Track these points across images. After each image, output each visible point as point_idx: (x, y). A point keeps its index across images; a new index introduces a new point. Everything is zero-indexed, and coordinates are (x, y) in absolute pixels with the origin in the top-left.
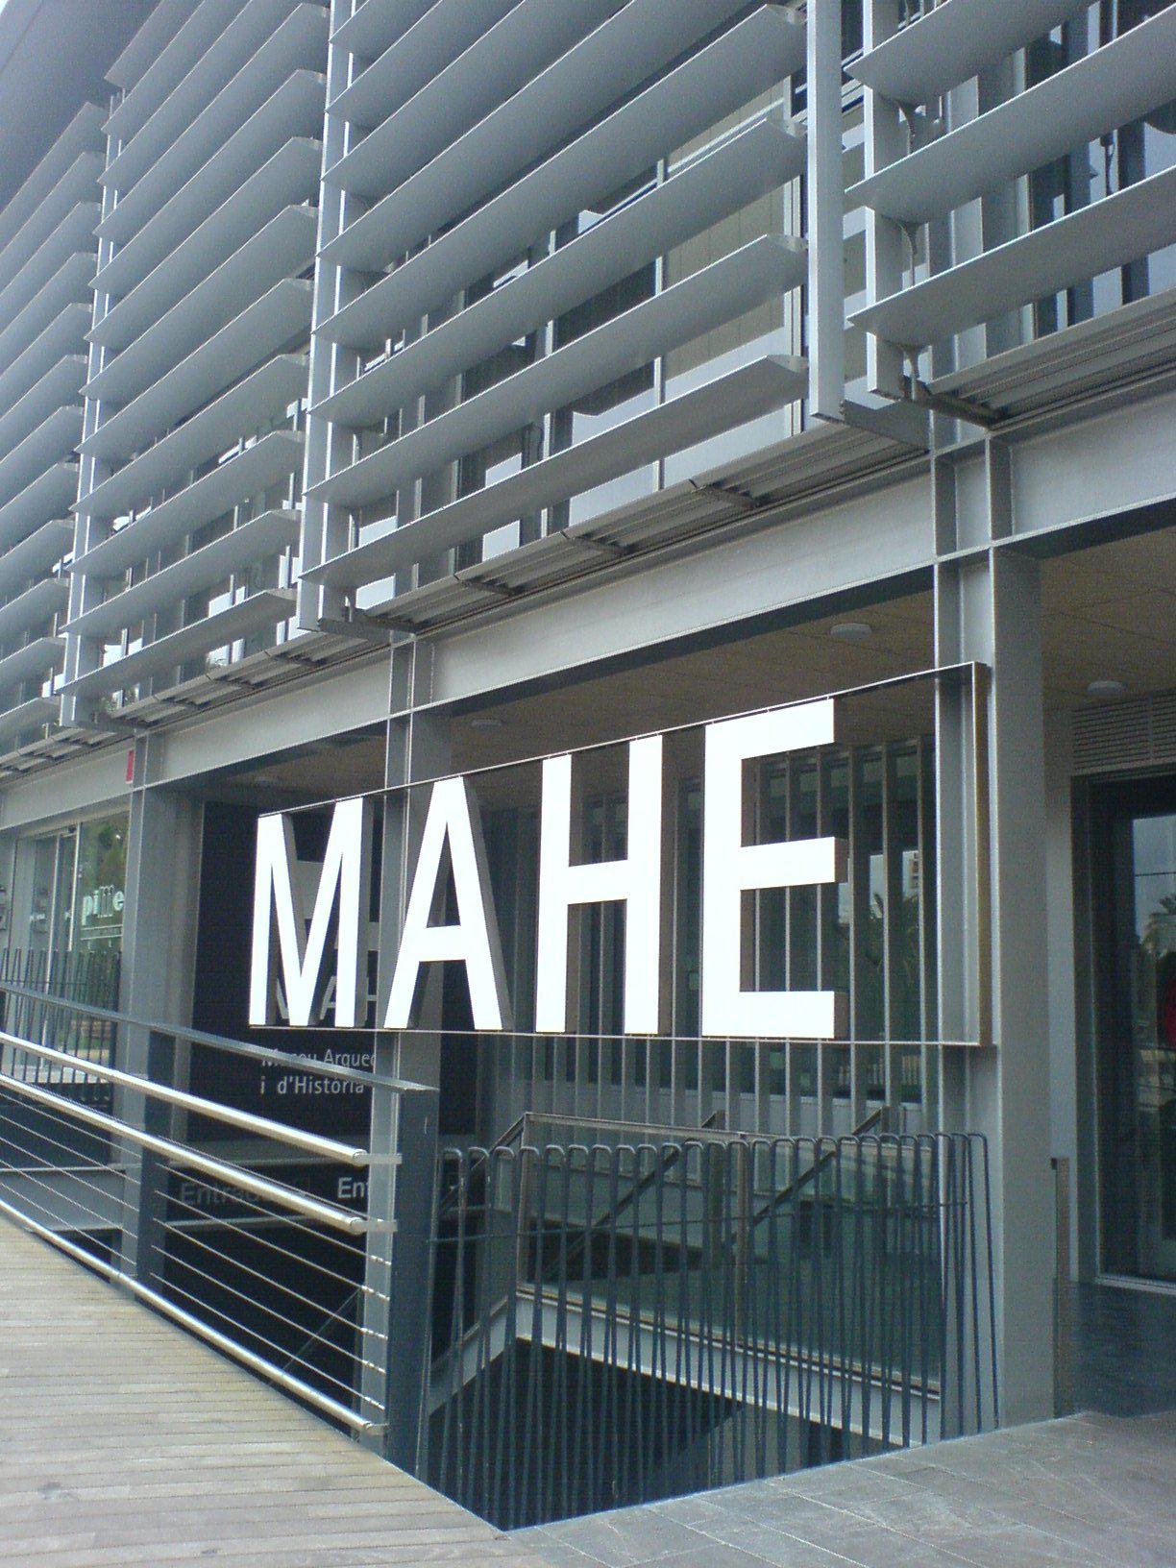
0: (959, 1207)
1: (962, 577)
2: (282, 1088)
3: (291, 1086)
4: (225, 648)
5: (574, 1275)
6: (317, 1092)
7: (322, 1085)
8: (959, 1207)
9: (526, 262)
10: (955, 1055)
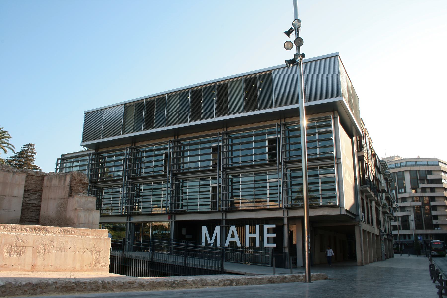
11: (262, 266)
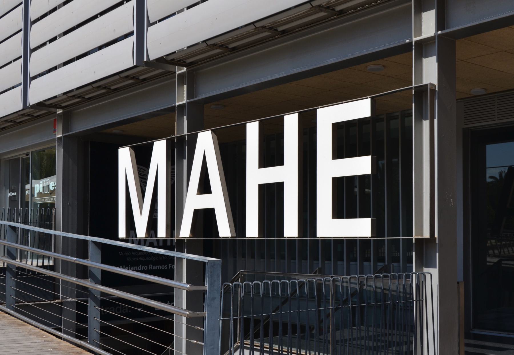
0: (421, 301)
4: (33, 100)
5: (256, 336)
6: (166, 268)
8: (421, 301)
10: (420, 241)
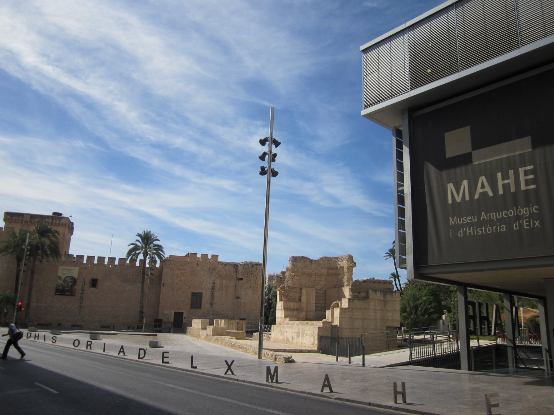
1: (387, 294)
2: (460, 234)
3: (465, 233)
7: (482, 230)
9: (548, 349)
11: (458, 326)
